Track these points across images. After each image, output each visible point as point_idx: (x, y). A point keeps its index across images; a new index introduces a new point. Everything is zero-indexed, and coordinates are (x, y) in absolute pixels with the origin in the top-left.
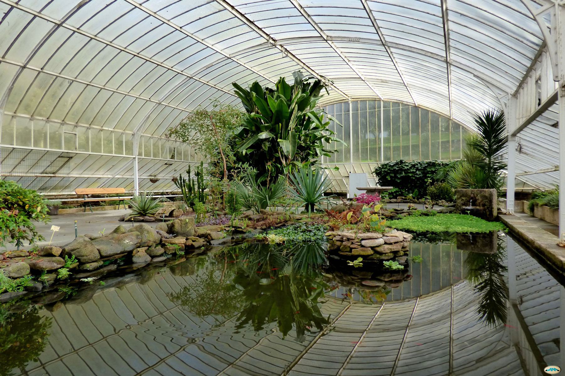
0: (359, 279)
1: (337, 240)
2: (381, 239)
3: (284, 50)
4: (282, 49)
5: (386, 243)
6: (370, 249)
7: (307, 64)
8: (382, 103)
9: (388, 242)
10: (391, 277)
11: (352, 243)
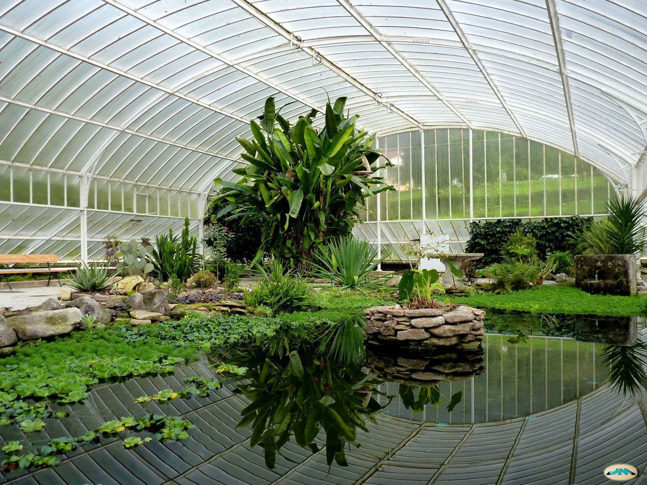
0: (408, 370)
1: (377, 320)
2: (441, 317)
3: (315, 55)
4: (312, 53)
5: (447, 323)
6: (423, 331)
7: (352, 75)
8: (471, 132)
9: (450, 321)
10: (454, 367)
11: (398, 323)
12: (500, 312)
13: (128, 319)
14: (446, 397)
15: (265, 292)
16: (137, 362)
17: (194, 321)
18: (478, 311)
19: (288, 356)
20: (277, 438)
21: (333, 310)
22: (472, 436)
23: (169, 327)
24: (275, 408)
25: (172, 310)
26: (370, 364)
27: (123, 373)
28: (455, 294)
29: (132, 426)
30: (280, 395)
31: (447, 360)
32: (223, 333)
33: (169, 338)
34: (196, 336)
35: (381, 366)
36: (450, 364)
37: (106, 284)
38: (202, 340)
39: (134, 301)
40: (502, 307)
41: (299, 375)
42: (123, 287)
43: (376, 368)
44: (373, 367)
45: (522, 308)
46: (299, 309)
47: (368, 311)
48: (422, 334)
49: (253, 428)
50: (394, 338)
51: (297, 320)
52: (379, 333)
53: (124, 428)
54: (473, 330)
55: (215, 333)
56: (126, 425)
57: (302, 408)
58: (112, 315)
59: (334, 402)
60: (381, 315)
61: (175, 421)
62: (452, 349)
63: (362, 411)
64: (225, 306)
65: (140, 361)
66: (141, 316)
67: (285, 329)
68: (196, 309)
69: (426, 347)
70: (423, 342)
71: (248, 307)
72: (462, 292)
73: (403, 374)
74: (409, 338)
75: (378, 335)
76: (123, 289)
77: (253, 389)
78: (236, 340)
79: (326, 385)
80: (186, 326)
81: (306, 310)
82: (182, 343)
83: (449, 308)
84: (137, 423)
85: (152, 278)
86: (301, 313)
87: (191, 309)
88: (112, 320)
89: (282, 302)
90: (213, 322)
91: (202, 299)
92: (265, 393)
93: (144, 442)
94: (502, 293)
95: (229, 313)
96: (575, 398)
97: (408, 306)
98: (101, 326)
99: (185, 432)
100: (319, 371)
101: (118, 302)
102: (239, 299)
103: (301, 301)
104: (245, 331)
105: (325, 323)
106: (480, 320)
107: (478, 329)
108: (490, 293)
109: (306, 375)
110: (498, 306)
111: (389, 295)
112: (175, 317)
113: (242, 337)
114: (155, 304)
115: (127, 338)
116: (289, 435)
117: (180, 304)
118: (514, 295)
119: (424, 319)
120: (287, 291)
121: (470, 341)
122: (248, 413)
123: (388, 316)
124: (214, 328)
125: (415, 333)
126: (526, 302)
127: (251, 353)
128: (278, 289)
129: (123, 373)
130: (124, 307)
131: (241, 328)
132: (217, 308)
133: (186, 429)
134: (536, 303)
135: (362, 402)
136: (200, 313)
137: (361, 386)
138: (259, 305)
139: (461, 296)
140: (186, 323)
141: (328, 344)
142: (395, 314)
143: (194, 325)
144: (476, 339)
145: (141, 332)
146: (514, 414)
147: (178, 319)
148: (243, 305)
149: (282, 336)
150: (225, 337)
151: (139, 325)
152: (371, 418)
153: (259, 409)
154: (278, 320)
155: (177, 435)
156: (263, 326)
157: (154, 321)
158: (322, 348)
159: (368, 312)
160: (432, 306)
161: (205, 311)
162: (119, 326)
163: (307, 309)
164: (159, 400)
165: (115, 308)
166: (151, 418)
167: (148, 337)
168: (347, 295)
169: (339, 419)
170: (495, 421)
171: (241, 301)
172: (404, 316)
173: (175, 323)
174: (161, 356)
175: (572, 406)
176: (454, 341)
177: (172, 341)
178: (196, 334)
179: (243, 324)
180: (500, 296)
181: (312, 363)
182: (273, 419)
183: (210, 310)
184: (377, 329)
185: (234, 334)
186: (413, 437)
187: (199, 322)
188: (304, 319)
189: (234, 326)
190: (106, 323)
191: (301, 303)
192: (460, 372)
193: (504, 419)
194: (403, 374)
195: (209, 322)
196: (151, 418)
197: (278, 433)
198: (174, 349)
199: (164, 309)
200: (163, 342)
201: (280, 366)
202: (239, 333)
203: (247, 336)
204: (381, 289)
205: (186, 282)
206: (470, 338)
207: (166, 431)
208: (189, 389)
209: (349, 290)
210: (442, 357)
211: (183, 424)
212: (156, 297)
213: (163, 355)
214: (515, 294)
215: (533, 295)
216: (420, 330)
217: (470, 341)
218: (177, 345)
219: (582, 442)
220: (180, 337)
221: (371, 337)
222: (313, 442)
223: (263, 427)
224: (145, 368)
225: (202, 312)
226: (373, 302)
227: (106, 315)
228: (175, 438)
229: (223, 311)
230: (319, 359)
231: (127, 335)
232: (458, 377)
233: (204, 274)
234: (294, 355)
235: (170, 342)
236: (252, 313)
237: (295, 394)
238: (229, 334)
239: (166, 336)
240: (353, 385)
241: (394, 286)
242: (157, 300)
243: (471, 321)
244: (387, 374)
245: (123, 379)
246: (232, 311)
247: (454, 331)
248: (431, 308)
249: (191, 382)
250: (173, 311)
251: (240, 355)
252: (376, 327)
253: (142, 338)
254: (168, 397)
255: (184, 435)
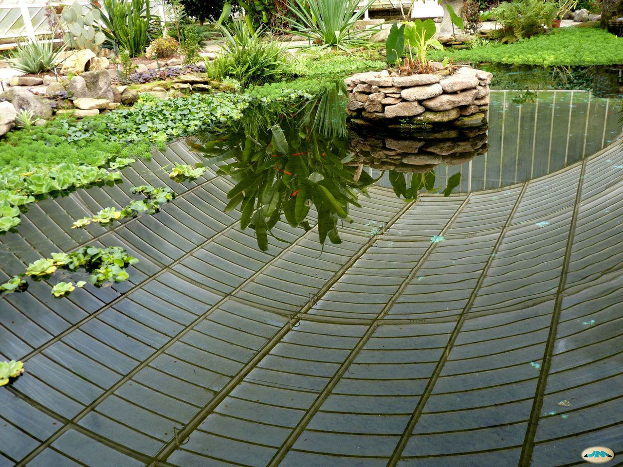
0: (398, 154)
1: (360, 92)
5: (445, 92)
6: (416, 104)
9: (448, 89)
11: (386, 96)
12: (507, 67)
13: (70, 111)
14: (442, 182)
15: (230, 61)
16: (79, 170)
17: (147, 107)
18: (483, 73)
19: (270, 130)
20: (267, 219)
21: (311, 78)
22: (468, 205)
23: (119, 117)
24: (262, 187)
25: (122, 94)
26: (354, 148)
27: (63, 185)
28: (455, 46)
29: (64, 265)
30: (266, 175)
31: (445, 140)
32: (181, 120)
33: (119, 131)
34: (149, 127)
35: (367, 150)
36: (449, 144)
37: (56, 62)
38: (157, 132)
39: (75, 88)
40: (510, 60)
41: (283, 151)
42: (73, 66)
43: (362, 152)
44: (358, 150)
45: (534, 61)
46: (271, 79)
47: (348, 80)
48: (414, 109)
49: (241, 210)
50: (381, 115)
51: (271, 94)
52: (363, 109)
53: (55, 268)
54: (477, 99)
55: (172, 120)
56: (59, 263)
57: (289, 187)
58: (52, 108)
59: (323, 178)
60: (365, 85)
61: (114, 255)
62: (450, 125)
63: (353, 186)
64: (186, 82)
65: (84, 167)
66: (87, 105)
67: (254, 107)
68: (151, 90)
69: (420, 124)
70: (415, 118)
71: (212, 82)
72: (463, 43)
73: (393, 159)
74: (399, 115)
75: (362, 112)
76: (74, 67)
77: (236, 169)
78: (196, 128)
79: (315, 161)
80: (138, 115)
81: (280, 81)
82: (134, 136)
83: (447, 72)
84: (71, 260)
85: (107, 50)
86: (274, 85)
87: (145, 90)
88: (54, 114)
89: (250, 73)
90: (170, 106)
91: (158, 76)
92: (250, 172)
93: (77, 288)
94: (510, 42)
95: (190, 91)
96: (580, 159)
97: (398, 72)
98: (41, 122)
99: (124, 271)
100: (304, 145)
101: (59, 90)
102: (201, 71)
103: (274, 69)
104: (207, 115)
105: (301, 97)
106: (485, 86)
107: (483, 98)
108: (496, 42)
109: (292, 151)
110: (505, 60)
111: (377, 54)
112: (127, 102)
113: (204, 123)
114: (101, 89)
115: (70, 135)
116: (280, 214)
117: (133, 84)
118: (525, 45)
119: (416, 89)
120: (255, 57)
121: (472, 114)
122: (234, 196)
123: (373, 87)
124: (170, 114)
125: (406, 108)
126: (540, 53)
127: (220, 138)
128: (244, 56)
129: (63, 185)
130: (66, 96)
131: (202, 111)
132: (176, 86)
133: (126, 265)
134: (550, 53)
135: (353, 176)
136: (153, 96)
137: (351, 159)
138: (225, 78)
139: (462, 49)
140: (138, 110)
141: (312, 113)
142: (382, 84)
143: (147, 112)
144: (480, 110)
145: (85, 127)
146: (513, 179)
147: (131, 104)
148: (206, 79)
149: (255, 114)
150: (184, 125)
151: (86, 117)
152: (364, 192)
153: (246, 190)
154: (246, 96)
155: (115, 276)
156: (228, 108)
157: (102, 110)
158: (306, 119)
159: (350, 83)
160: (427, 70)
161: (162, 91)
162: (62, 121)
163: (281, 78)
164: (100, 223)
165: (55, 97)
166: (85, 254)
167: (95, 132)
168: (328, 56)
169: (330, 196)
170: (493, 188)
171: (203, 75)
172: (393, 86)
173: (125, 111)
174: (109, 158)
175: (576, 168)
176: (453, 115)
177: (124, 135)
178: (150, 124)
179: (205, 105)
180: (508, 46)
181: (296, 137)
182: (262, 199)
183: (168, 90)
184: (361, 104)
185: (194, 120)
186: (408, 209)
187: (154, 107)
188: (277, 93)
189: (194, 110)
190: (47, 118)
191: (273, 72)
192: (460, 153)
193: (502, 186)
194: (393, 159)
195: (164, 108)
196: (85, 254)
197: (268, 213)
198: (124, 146)
199: (112, 94)
200: (113, 138)
201: (263, 142)
202: (200, 118)
203: (209, 121)
204: (367, 45)
205: (145, 52)
206: (472, 109)
207: (102, 270)
208: (135, 204)
209: (330, 49)
210: (438, 136)
211: (123, 259)
212: (100, 80)
213: (110, 156)
214: (526, 43)
215: (547, 42)
216: (413, 103)
217: (472, 114)
218: (129, 140)
219: (583, 207)
220: (131, 130)
221: (354, 114)
222: (305, 220)
223: (251, 209)
224: (88, 177)
225: (157, 93)
226: (358, 63)
227: (45, 107)
228: (111, 280)
229: (183, 89)
230: (304, 132)
231: (70, 132)
232: (457, 160)
233: (165, 40)
234: (277, 129)
235: (121, 136)
236: (217, 88)
237: (281, 172)
238: (189, 120)
239: (115, 129)
240: (342, 158)
241: (383, 41)
242: (102, 83)
243: (475, 88)
244: (374, 160)
245: (66, 192)
246: (196, 88)
247: (454, 102)
248: (427, 73)
249: (140, 192)
250: (123, 96)
251: (218, 132)
252: (359, 101)
253: (87, 135)
254: (110, 218)
255: (123, 275)
